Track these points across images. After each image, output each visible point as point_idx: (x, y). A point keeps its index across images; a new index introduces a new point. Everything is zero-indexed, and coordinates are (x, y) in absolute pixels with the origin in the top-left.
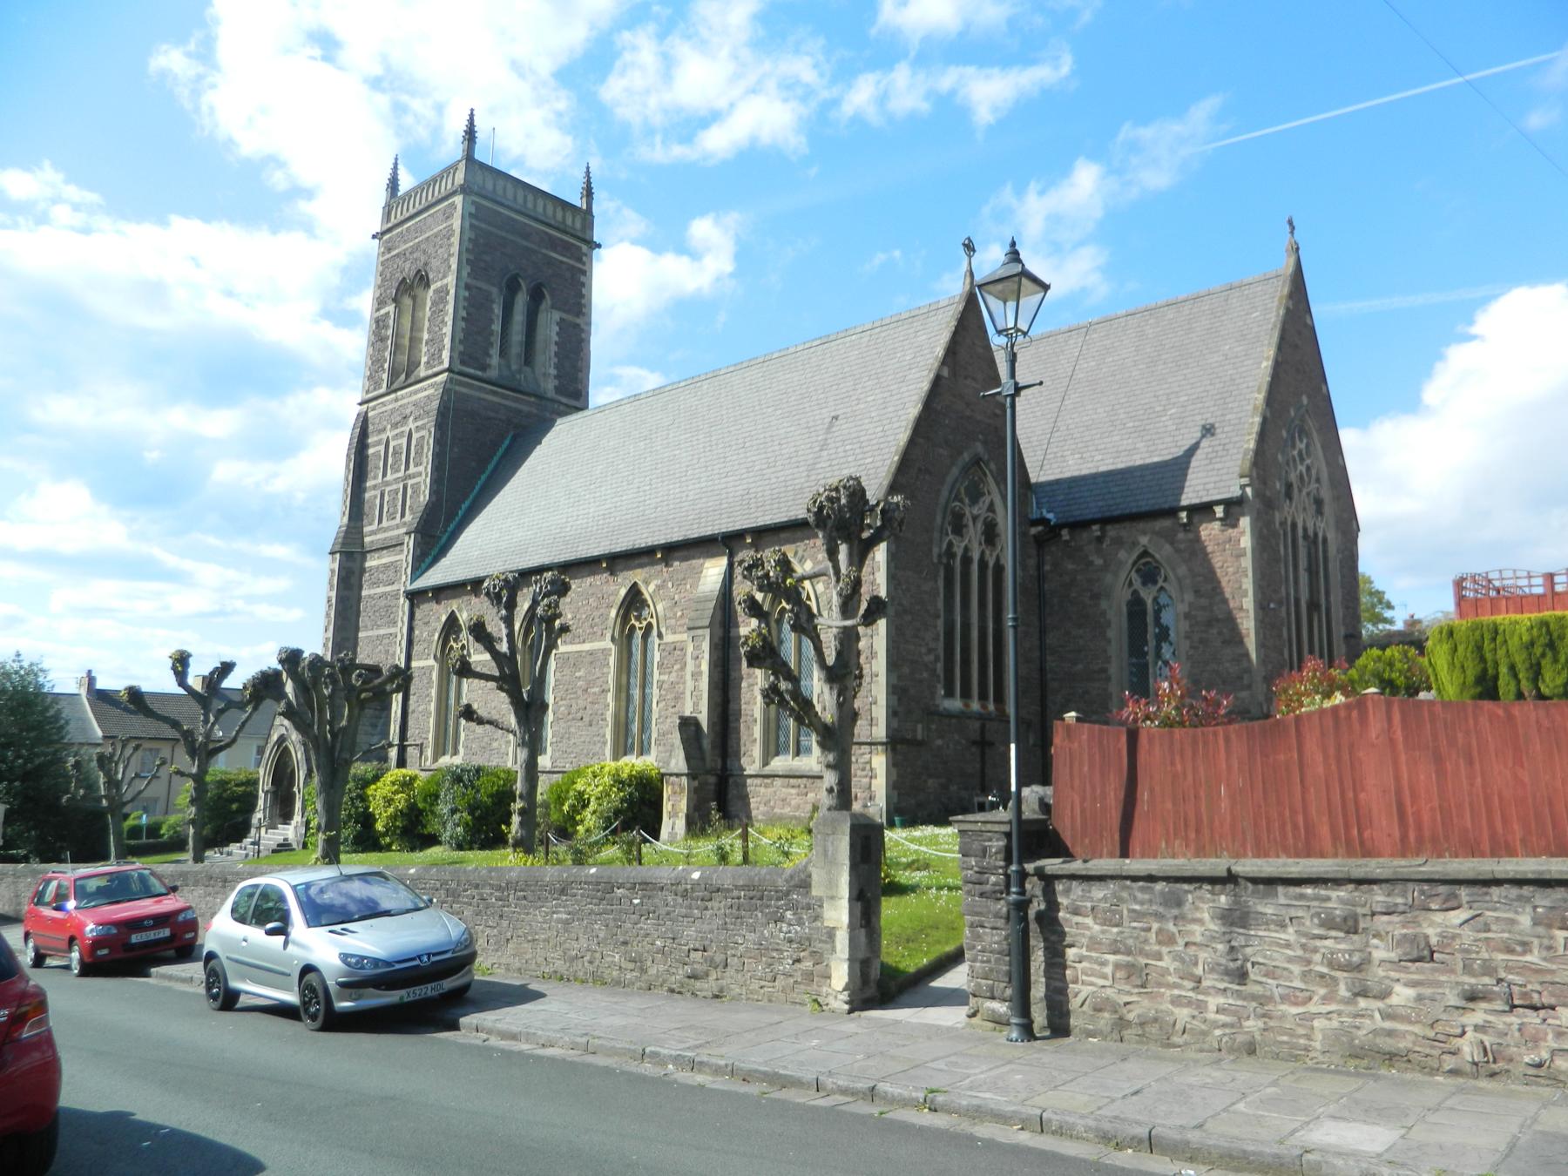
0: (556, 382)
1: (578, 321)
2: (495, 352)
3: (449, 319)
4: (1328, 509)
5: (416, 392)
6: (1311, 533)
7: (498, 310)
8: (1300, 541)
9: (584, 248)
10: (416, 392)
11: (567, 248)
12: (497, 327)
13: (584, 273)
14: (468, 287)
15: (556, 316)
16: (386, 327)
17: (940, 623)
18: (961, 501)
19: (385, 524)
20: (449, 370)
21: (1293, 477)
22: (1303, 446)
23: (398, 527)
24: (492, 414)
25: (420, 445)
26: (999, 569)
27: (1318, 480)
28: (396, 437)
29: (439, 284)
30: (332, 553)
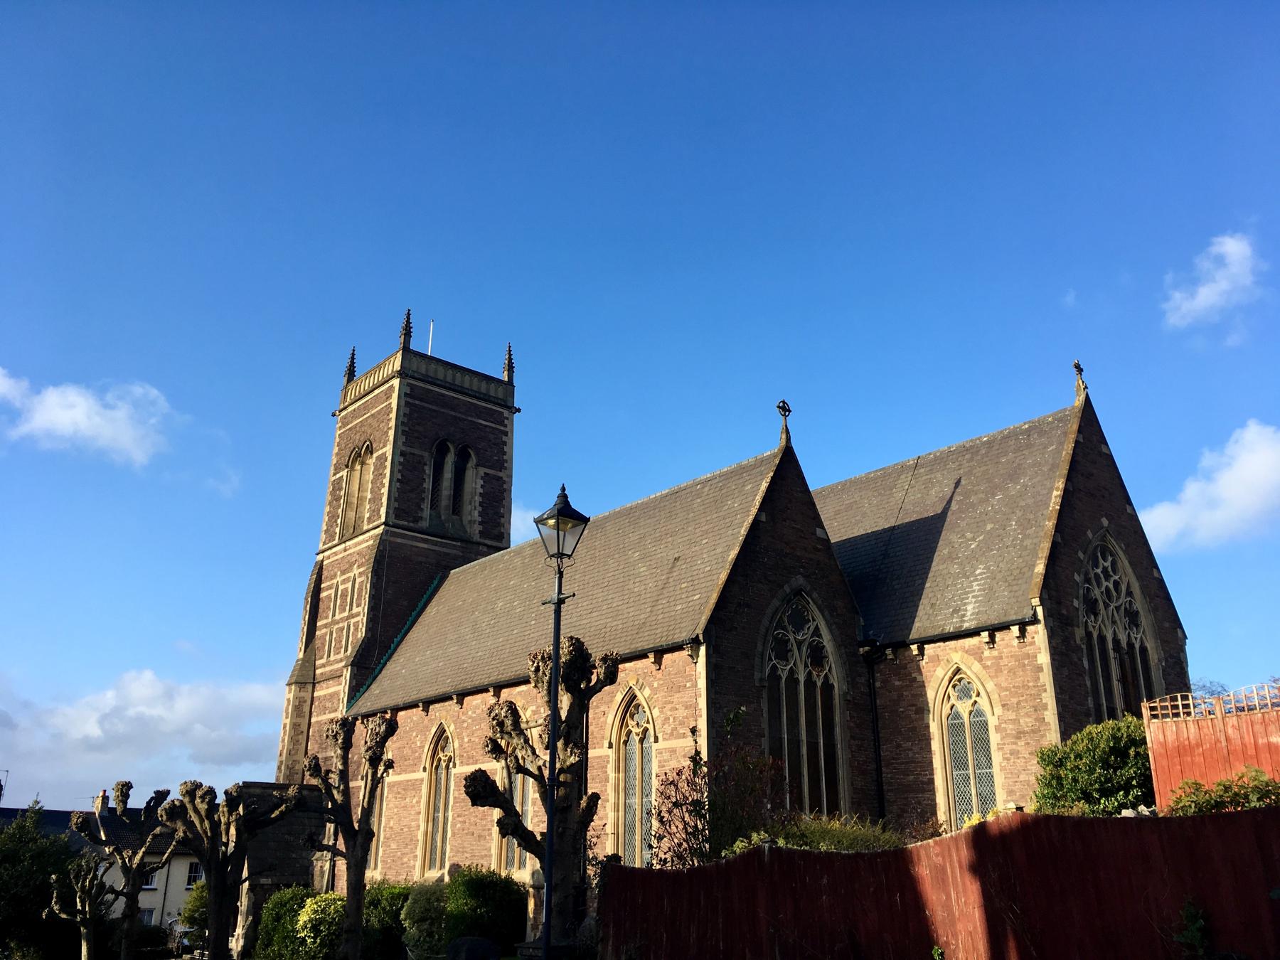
0: (481, 528)
1: (501, 474)
2: (426, 506)
3: (386, 481)
4: (1145, 620)
5: (360, 544)
6: (1124, 644)
7: (429, 470)
8: (1112, 654)
9: (506, 413)
10: (360, 544)
11: (490, 415)
12: (428, 485)
13: (506, 434)
14: (402, 454)
15: (482, 471)
16: (340, 489)
17: (765, 743)
18: (784, 628)
19: (332, 658)
20: (385, 524)
21: (1096, 593)
22: (1108, 564)
23: (341, 660)
24: (423, 559)
25: (360, 589)
26: (827, 687)
27: (1129, 593)
28: (344, 582)
29: (380, 452)
30: (289, 684)
